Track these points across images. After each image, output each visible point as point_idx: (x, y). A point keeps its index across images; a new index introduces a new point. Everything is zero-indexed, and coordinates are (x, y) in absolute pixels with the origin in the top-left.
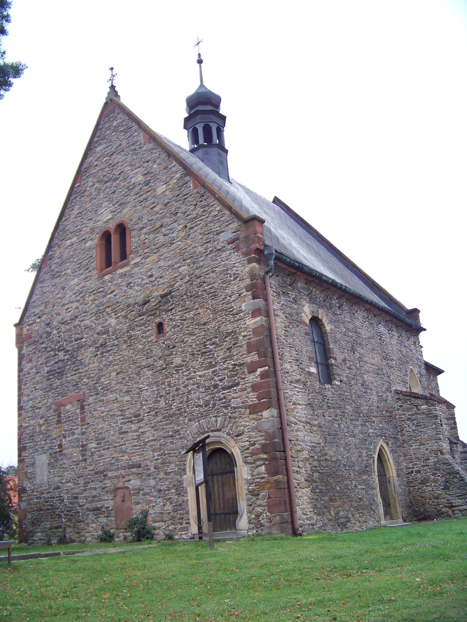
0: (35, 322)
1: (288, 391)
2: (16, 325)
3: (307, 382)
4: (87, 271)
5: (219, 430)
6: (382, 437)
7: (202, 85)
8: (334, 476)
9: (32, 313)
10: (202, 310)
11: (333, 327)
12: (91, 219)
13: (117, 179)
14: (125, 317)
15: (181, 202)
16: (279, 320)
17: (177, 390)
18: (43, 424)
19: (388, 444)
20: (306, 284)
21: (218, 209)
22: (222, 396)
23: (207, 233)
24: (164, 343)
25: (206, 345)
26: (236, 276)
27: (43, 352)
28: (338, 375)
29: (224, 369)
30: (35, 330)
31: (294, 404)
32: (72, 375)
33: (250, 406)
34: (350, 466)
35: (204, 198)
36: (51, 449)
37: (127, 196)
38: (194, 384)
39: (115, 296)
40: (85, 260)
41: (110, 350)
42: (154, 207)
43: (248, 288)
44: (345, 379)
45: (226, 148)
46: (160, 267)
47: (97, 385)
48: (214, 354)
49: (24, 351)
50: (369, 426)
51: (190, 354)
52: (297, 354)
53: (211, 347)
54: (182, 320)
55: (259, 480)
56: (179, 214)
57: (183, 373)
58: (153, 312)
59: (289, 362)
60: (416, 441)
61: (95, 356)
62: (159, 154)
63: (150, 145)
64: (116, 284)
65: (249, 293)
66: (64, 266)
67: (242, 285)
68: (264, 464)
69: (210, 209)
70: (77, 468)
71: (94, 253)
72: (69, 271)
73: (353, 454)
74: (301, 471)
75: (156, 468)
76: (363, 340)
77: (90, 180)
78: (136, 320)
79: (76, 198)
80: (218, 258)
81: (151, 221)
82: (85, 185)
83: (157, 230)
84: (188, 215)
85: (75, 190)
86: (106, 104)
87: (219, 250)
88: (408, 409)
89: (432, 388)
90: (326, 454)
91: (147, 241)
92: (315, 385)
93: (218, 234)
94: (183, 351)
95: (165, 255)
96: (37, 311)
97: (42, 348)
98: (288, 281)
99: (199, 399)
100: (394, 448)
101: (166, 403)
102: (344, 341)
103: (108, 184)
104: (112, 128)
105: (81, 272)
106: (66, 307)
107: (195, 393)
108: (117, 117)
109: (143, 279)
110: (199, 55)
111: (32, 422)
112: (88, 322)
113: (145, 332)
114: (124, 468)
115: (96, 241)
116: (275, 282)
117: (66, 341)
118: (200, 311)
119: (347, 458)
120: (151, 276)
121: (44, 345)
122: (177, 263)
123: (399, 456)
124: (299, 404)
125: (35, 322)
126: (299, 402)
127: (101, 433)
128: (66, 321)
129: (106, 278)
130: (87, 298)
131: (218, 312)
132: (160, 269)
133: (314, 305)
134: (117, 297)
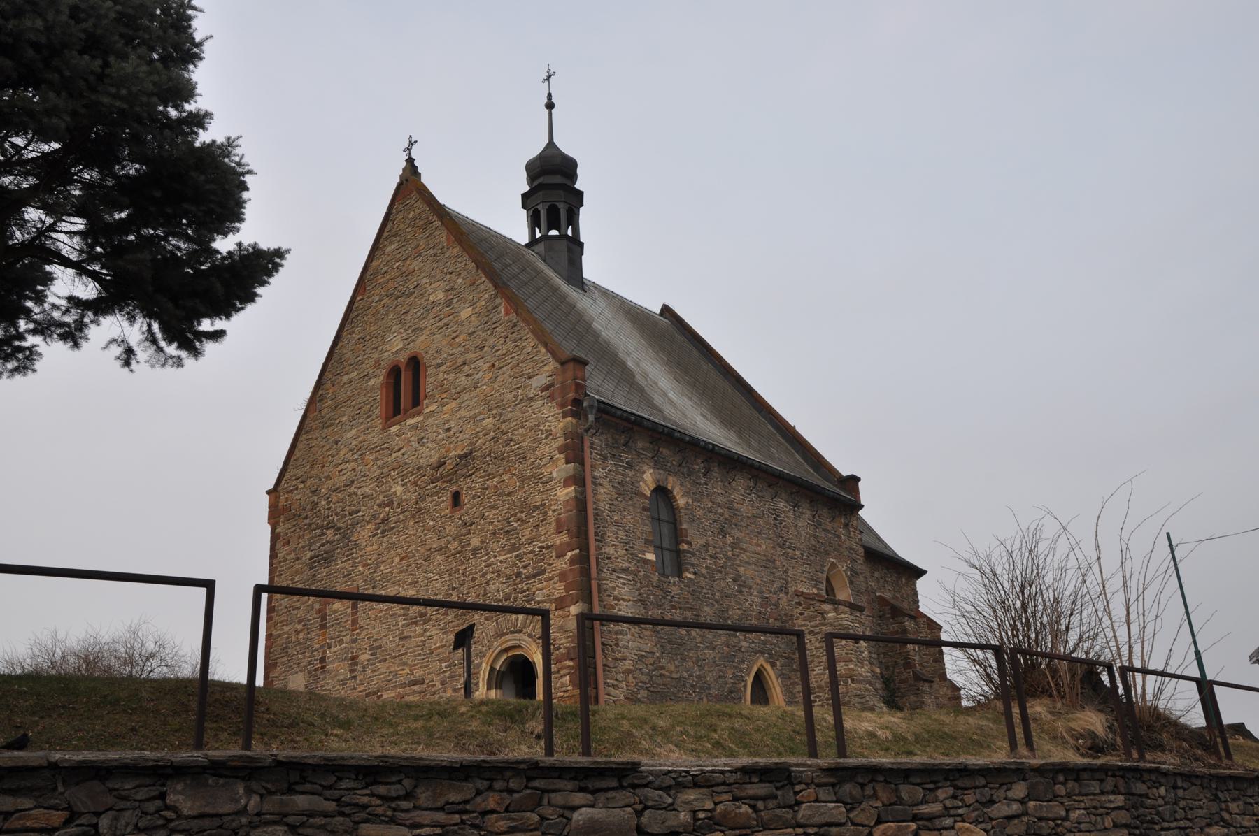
0: (297, 489)
1: (608, 582)
2: (268, 492)
3: (640, 571)
4: (369, 420)
5: (520, 631)
6: (763, 653)
7: (551, 143)
8: (673, 698)
9: (292, 476)
10: (507, 477)
11: (690, 501)
12: (376, 348)
13: (412, 294)
14: (415, 484)
15: (489, 332)
16: (602, 490)
17: (473, 580)
18: (302, 630)
19: (773, 665)
20: (651, 443)
21: (532, 344)
22: (525, 588)
23: (517, 375)
24: (460, 519)
25: (509, 522)
26: (549, 434)
27: (305, 530)
28: (693, 565)
29: (529, 553)
30: (297, 500)
31: (615, 598)
32: (342, 562)
33: (556, 599)
34: (701, 688)
35: (517, 328)
36: (309, 665)
37: (423, 319)
38: (493, 573)
39: (403, 455)
40: (367, 404)
41: (394, 527)
42: (457, 336)
43: (562, 450)
44: (704, 571)
45: (582, 240)
46: (459, 419)
47: (375, 575)
48: (518, 534)
49: (278, 530)
50: (741, 637)
51: (491, 534)
52: (626, 535)
53: (516, 524)
54: (484, 489)
55: (562, 694)
56: (486, 349)
57: (481, 557)
58: (450, 478)
59: (613, 545)
60: (820, 663)
61: (374, 536)
62: (466, 265)
63: (455, 250)
64: (405, 439)
65: (562, 456)
66: (339, 411)
67: (556, 445)
68: (569, 673)
69: (523, 344)
70: (343, 689)
71: (378, 395)
72: (345, 418)
73: (709, 672)
74: (620, 685)
75: (443, 683)
76: (741, 519)
77: (377, 292)
78: (429, 487)
79: (357, 316)
80: (529, 409)
81: (452, 355)
82: (370, 300)
83: (458, 369)
84: (497, 351)
85: (356, 304)
86: (400, 185)
87: (531, 398)
88: (811, 618)
89: (902, 597)
90: (663, 668)
91: (445, 382)
92: (652, 576)
93: (530, 378)
94: (483, 529)
95: (466, 403)
96: (300, 473)
97: (305, 525)
98: (622, 439)
99: (498, 591)
100: (784, 672)
101: (459, 597)
102: (707, 520)
103: (399, 300)
104: (407, 221)
105: (361, 420)
106: (339, 469)
107: (494, 583)
108: (415, 205)
109: (440, 433)
110: (550, 95)
111: (286, 629)
112: (366, 490)
113: (438, 504)
114: (404, 685)
115: (382, 378)
116: (601, 441)
117: (337, 514)
118: (505, 477)
119: (699, 677)
120: (449, 430)
121: (307, 521)
122: (480, 413)
123: (794, 684)
124: (623, 599)
125: (297, 489)
126: (624, 597)
127: (377, 640)
128: (339, 488)
129: (393, 429)
130: (367, 457)
131: (526, 479)
132: (460, 421)
133: (661, 471)
134: (406, 456)
